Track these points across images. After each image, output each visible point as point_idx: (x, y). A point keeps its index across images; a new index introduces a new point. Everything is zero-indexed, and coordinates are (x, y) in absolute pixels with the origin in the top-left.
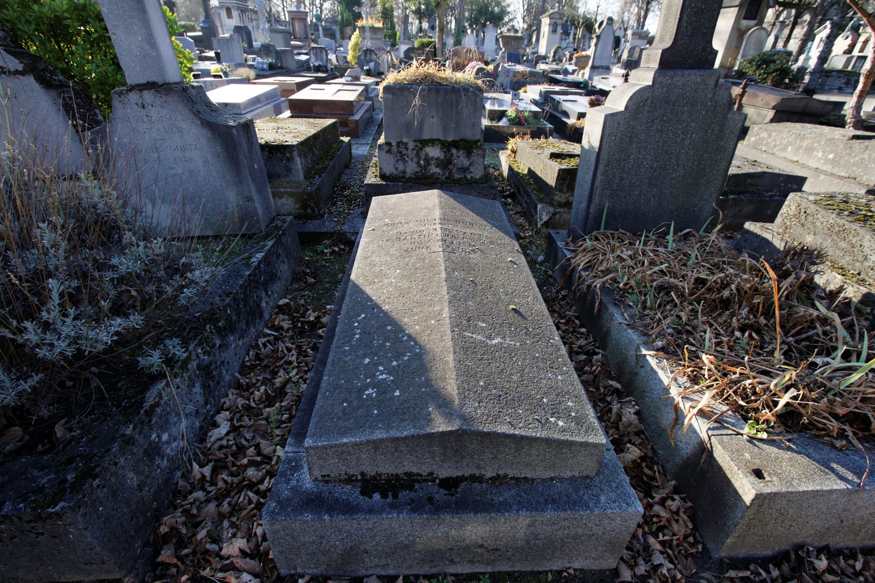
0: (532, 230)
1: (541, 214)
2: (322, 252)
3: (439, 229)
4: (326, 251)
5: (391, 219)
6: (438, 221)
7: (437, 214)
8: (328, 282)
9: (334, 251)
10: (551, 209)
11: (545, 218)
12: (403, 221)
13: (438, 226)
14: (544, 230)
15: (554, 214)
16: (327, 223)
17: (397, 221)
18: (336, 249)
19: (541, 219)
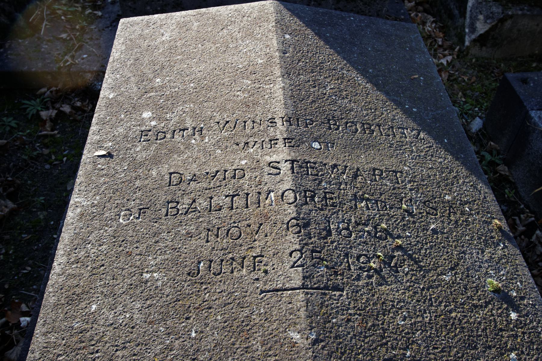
0: (451, 48)
1: (474, 19)
2: (37, 116)
3: (285, 167)
4: (44, 114)
5: (160, 112)
6: (280, 130)
7: (276, 96)
8: (43, 207)
9: (61, 114)
10: (496, 9)
11: (482, 28)
12: (189, 123)
13: (281, 154)
14: (475, 51)
15: (502, 21)
16: (45, 47)
17: (173, 118)
18: (66, 109)
19: (473, 29)
